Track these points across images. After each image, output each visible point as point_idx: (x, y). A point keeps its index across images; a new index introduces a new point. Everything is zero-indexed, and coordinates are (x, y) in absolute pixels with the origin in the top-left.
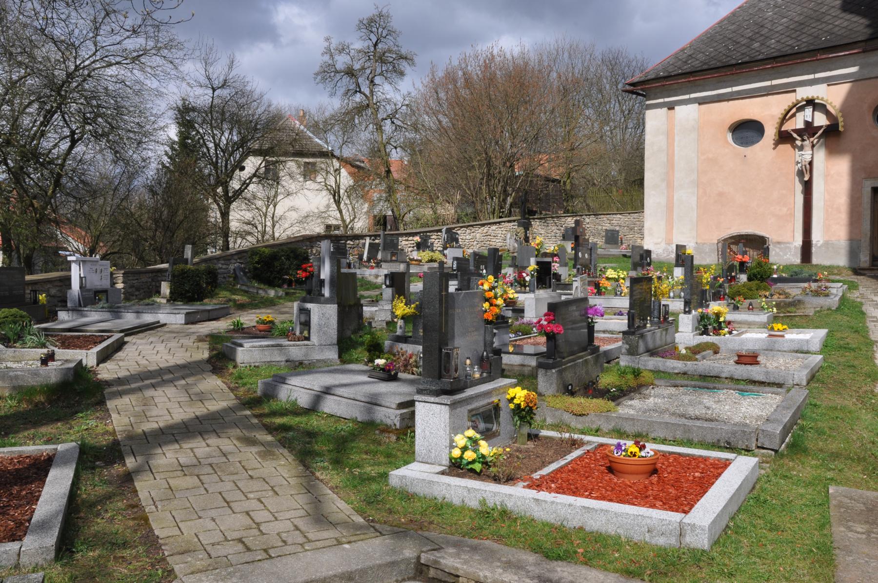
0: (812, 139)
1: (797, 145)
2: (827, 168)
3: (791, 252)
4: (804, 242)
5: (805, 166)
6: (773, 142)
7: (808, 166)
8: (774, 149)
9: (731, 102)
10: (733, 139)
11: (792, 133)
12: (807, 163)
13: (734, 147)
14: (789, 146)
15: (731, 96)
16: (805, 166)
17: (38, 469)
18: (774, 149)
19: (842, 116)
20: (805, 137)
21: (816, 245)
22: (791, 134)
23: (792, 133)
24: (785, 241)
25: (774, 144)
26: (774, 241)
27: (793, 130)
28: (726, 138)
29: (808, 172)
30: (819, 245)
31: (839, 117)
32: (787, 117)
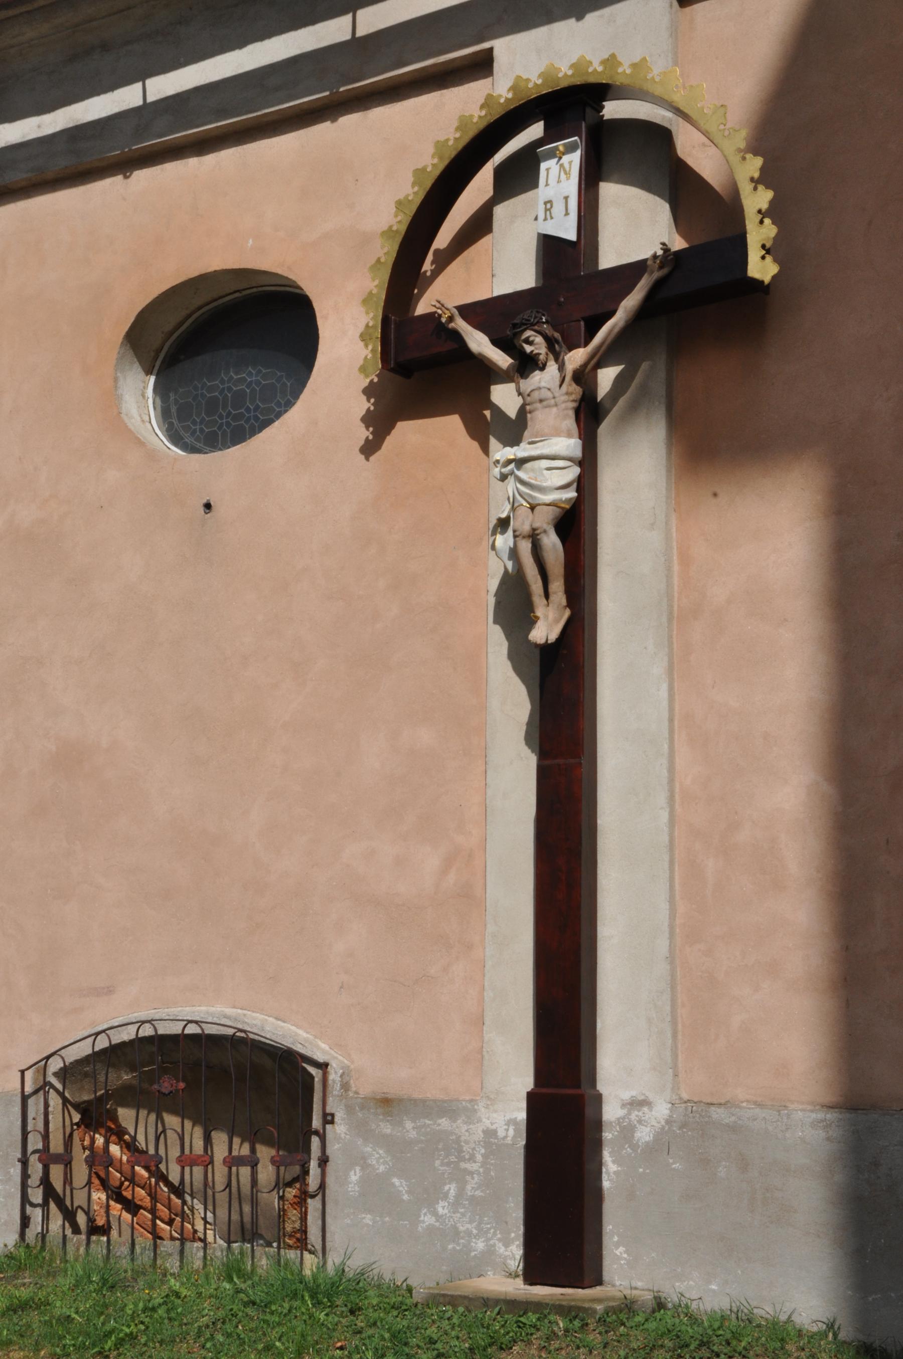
0: (576, 357)
1: (498, 412)
2: (685, 560)
3: (461, 1177)
4: (181, 1177)
5: (534, 537)
6: (363, 405)
7: (551, 541)
8: (369, 449)
9: (143, 177)
10: (165, 414)
11: (461, 325)
12: (544, 520)
13: (152, 456)
14: (453, 424)
15: (141, 132)
16: (534, 537)
17: (145, 1274)
18: (369, 449)
19: (764, 179)
20: (537, 345)
21: (627, 1131)
22: (456, 336)
23: (461, 325)
24: (431, 1092)
25: (368, 419)
26: (364, 1087)
27: (470, 312)
28: (112, 400)
29: (557, 586)
30: (644, 1135)
31: (745, 188)
32: (443, 238)
